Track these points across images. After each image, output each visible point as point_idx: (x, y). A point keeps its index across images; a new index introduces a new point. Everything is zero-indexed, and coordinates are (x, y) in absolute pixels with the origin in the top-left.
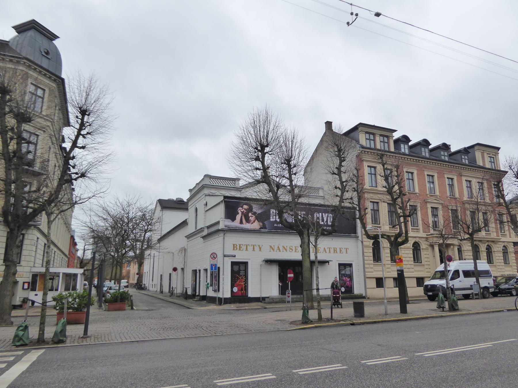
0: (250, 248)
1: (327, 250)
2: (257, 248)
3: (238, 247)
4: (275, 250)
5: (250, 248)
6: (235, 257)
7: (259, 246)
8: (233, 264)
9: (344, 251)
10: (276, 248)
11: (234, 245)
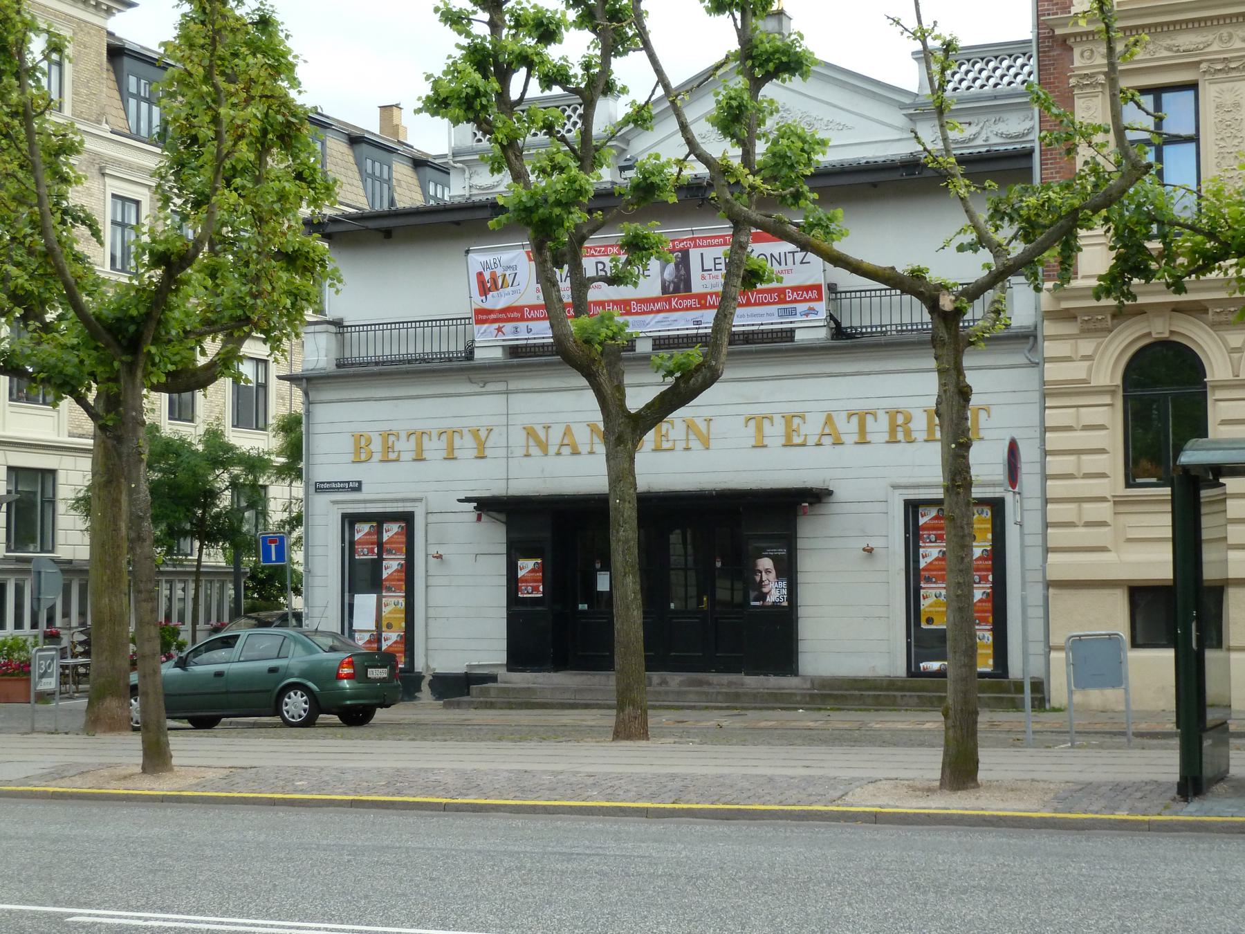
0: (434, 448)
1: (849, 429)
2: (466, 444)
3: (376, 446)
4: (552, 450)
5: (434, 448)
6: (358, 487)
7: (475, 433)
8: (350, 520)
9: (405, 447)
10: (556, 436)
11: (358, 437)
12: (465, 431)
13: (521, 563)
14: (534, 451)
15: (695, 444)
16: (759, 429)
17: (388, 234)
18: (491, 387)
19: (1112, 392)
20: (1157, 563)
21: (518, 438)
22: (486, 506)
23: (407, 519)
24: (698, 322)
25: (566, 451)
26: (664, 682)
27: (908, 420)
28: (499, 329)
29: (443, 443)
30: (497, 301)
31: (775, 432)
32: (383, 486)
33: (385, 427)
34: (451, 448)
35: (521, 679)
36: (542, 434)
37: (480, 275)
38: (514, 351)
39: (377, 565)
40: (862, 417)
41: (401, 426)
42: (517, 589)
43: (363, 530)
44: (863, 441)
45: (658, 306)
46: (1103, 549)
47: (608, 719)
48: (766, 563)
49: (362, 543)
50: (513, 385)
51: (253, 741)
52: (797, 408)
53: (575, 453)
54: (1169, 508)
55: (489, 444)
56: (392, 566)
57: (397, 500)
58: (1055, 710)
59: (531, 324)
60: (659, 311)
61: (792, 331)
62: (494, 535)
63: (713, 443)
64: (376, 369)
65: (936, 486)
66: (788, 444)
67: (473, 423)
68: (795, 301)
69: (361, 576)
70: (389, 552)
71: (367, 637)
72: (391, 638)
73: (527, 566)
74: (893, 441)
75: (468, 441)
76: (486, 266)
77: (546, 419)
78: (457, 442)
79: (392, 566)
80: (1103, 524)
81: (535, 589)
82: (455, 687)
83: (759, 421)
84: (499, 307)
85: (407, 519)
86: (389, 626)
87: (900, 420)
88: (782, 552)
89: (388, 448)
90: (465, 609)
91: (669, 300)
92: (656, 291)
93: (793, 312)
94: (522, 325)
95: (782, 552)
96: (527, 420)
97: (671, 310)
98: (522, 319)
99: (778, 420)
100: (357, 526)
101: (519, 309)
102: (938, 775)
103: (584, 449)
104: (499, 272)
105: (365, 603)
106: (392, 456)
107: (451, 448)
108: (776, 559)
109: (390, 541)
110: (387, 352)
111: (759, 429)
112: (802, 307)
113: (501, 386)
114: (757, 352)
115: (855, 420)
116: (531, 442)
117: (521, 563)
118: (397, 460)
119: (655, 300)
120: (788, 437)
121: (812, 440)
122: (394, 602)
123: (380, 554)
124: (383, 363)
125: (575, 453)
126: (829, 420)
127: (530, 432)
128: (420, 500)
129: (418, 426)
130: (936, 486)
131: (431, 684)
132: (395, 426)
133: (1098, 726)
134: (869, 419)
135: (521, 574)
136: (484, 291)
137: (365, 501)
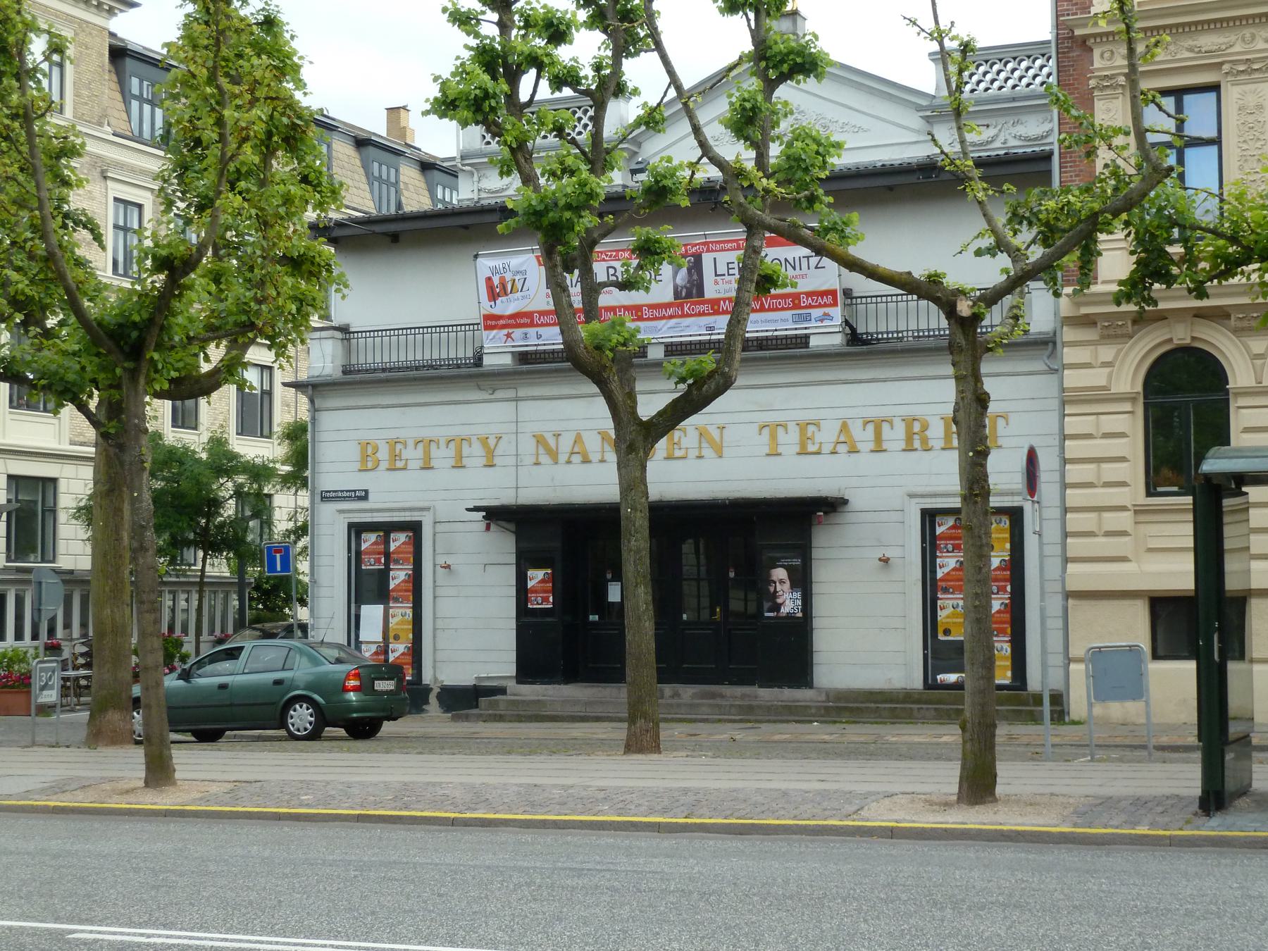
0: (442, 456)
1: (864, 437)
2: (474, 452)
3: (383, 454)
4: (563, 458)
5: (442, 456)
6: (365, 496)
7: (484, 441)
8: (357, 530)
9: (413, 455)
10: (566, 444)
11: (364, 445)
12: (474, 439)
13: (530, 573)
14: (544, 459)
15: (708, 452)
16: (773, 437)
17: (395, 238)
18: (500, 394)
19: (1132, 399)
20: (1178, 573)
21: (528, 446)
22: (495, 515)
23: (414, 528)
24: (711, 328)
25: (576, 459)
26: (676, 695)
27: (925, 427)
28: (508, 335)
29: (451, 451)
30: (506, 307)
31: (789, 440)
32: (390, 495)
33: (393, 434)
34: (459, 456)
35: (531, 691)
36: (552, 442)
37: (489, 280)
38: (524, 358)
39: (384, 575)
40: (878, 425)
41: (409, 434)
42: (527, 600)
43: (369, 539)
44: (879, 449)
45: (670, 311)
46: (1124, 559)
47: (619, 732)
48: (780, 574)
49: (368, 553)
50: (522, 392)
51: (257, 755)
52: (812, 415)
53: (586, 461)
54: (1190, 517)
55: (498, 452)
56: (399, 576)
57: (404, 510)
58: (1074, 723)
59: (541, 330)
60: (671, 317)
61: (807, 337)
62: (504, 545)
63: (726, 452)
64: (383, 375)
65: (954, 495)
66: (803, 452)
67: (482, 430)
68: (810, 306)
69: (367, 586)
70: (397, 562)
71: (373, 648)
72: (398, 649)
73: (536, 576)
74: (909, 449)
75: (477, 449)
76: (495, 270)
77: (556, 427)
78: (466, 450)
79: (399, 576)
80: (1124, 533)
81: (545, 600)
82: (463, 700)
83: (773, 429)
84: (508, 312)
85: (414, 528)
86: (396, 638)
87: (917, 427)
88: (797, 562)
89: (395, 457)
90: (473, 620)
91: (681, 306)
92: (668, 297)
93: (807, 318)
94: (532, 331)
95: (797, 562)
96: (537, 428)
97: (683, 316)
98: (532, 325)
99: (792, 428)
100: (363, 536)
101: (529, 315)
102: (955, 789)
103: (595, 457)
104: (508, 276)
105: (372, 614)
106: (400, 464)
107: (459, 456)
108: (790, 570)
109: (397, 551)
110: (394, 359)
111: (773, 437)
112: (816, 313)
113: (510, 393)
114: (771, 358)
115: (871, 427)
116: (541, 450)
117: (530, 573)
118: (404, 469)
119: (667, 306)
120: (803, 445)
121: (827, 448)
122: (401, 613)
123: (387, 564)
124: (390, 370)
125: (586, 461)
126: (844, 428)
127: (540, 440)
128: (428, 509)
129: (426, 433)
130: (954, 495)
131: (439, 697)
132: (402, 434)
133: (1118, 739)
134: (885, 426)
135: (530, 584)
136: (493, 296)
137: (372, 511)
